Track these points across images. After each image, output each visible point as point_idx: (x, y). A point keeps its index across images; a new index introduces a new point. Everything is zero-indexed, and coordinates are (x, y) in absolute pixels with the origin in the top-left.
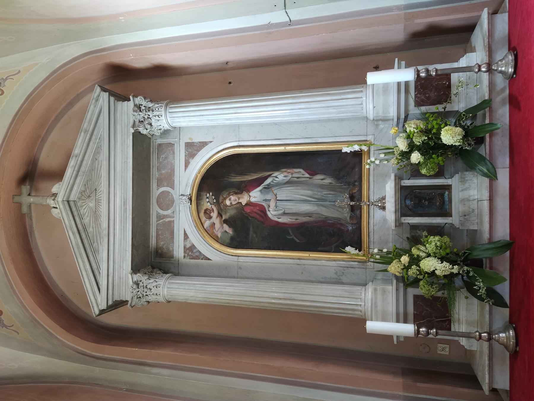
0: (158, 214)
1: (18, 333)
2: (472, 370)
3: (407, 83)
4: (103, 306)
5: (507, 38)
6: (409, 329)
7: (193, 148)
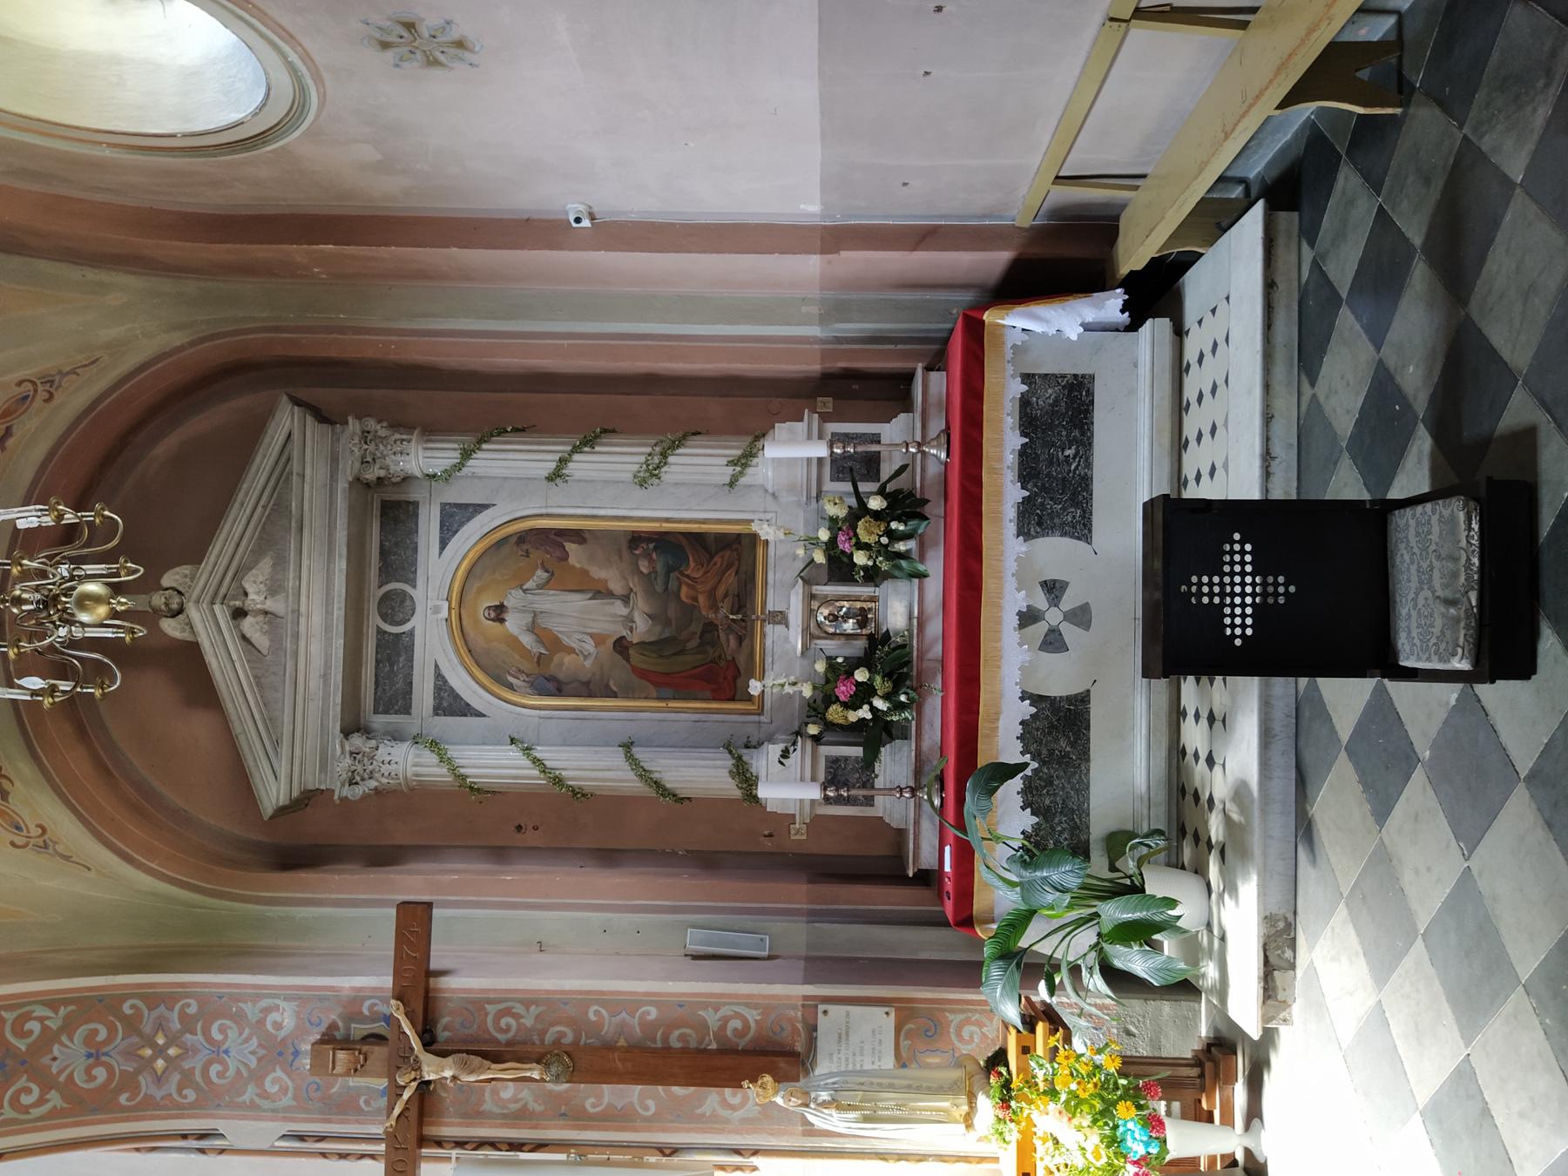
0: (380, 631)
3: (820, 460)
4: (283, 800)
7: (454, 518)
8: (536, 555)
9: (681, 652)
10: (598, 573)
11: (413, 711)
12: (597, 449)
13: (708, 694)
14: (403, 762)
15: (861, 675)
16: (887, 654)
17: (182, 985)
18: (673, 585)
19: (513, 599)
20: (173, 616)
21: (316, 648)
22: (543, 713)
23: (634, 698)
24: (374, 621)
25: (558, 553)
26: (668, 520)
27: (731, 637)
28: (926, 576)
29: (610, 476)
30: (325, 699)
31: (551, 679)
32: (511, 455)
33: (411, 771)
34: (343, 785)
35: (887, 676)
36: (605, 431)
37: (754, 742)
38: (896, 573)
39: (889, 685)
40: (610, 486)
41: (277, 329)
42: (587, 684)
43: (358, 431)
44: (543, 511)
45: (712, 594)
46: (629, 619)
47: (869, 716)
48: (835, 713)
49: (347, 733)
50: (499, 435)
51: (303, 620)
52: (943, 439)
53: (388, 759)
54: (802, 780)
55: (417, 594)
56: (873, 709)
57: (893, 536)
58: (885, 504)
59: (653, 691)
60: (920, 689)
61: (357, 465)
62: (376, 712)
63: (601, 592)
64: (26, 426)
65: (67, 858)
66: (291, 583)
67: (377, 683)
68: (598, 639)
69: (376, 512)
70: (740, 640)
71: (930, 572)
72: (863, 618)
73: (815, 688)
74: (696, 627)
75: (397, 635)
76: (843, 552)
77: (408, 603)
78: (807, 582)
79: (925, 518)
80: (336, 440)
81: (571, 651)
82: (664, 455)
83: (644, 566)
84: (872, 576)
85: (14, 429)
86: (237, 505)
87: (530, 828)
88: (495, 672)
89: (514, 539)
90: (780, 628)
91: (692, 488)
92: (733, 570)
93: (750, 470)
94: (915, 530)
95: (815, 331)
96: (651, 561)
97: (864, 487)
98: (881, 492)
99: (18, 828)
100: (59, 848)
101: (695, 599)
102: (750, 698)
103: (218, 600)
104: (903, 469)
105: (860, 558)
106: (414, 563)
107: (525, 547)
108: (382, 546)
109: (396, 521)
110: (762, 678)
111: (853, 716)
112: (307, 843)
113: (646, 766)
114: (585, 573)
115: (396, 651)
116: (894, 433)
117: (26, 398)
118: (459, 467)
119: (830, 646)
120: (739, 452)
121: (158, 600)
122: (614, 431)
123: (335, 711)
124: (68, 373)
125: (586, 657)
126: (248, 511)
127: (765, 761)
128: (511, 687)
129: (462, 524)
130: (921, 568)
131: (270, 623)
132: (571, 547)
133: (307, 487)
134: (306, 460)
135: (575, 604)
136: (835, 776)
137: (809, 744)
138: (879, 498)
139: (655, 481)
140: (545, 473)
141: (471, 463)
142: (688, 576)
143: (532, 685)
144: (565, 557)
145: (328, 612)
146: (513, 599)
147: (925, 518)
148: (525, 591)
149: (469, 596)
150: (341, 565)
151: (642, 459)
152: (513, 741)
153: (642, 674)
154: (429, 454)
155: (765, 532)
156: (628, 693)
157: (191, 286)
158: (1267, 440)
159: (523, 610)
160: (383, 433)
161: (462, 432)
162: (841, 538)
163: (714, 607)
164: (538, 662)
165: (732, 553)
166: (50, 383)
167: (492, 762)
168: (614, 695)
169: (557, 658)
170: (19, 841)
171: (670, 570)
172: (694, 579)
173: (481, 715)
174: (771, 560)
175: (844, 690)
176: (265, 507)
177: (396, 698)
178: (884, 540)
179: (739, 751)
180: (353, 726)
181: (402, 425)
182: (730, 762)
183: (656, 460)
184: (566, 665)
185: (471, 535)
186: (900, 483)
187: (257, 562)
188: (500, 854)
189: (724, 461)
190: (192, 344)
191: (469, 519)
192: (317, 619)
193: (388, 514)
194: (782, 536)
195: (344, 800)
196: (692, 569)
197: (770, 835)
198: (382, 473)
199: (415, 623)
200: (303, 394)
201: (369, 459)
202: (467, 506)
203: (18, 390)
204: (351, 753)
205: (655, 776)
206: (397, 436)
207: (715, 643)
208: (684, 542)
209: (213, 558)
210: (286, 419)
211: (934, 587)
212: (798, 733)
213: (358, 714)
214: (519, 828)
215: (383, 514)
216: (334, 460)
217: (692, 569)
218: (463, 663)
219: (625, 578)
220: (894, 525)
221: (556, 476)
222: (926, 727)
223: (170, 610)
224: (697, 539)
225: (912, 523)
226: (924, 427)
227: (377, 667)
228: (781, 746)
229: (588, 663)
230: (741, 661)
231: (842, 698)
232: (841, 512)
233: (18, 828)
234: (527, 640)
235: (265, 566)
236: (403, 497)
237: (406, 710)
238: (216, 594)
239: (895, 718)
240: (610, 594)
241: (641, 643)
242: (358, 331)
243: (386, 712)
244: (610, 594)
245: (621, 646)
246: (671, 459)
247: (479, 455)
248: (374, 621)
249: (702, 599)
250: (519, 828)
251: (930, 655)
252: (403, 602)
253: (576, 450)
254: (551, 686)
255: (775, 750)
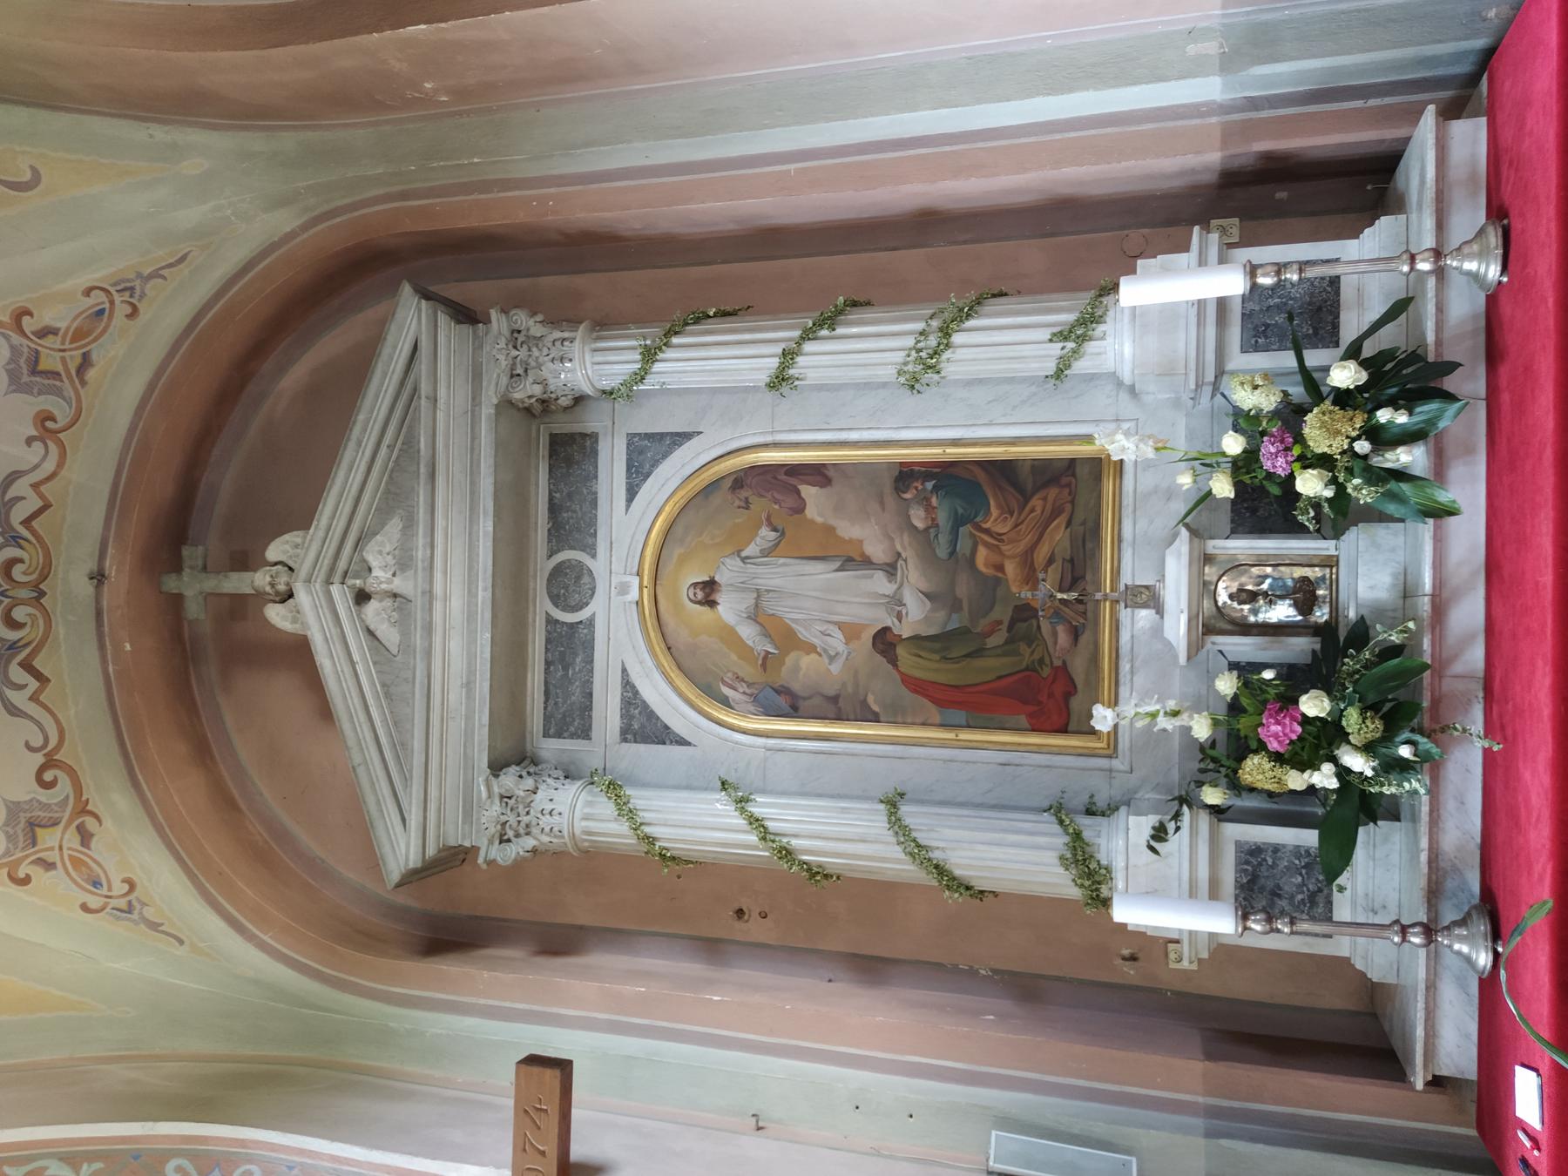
0: (551, 621)
1: (181, 942)
2: (1384, 1036)
3: (1222, 303)
4: (414, 861)
5: (1483, 323)
6: (1221, 922)
7: (646, 453)
8: (760, 505)
9: (978, 653)
10: (849, 530)
11: (594, 734)
12: (840, 331)
13: (1023, 720)
14: (570, 812)
15: (1314, 705)
16: (1368, 666)
17: (243, 1143)
18: (964, 546)
19: (728, 572)
20: (283, 601)
21: (456, 645)
22: (771, 742)
23: (905, 724)
24: (543, 606)
25: (790, 502)
26: (955, 443)
27: (1060, 629)
28: (1451, 512)
29: (860, 375)
30: (469, 717)
31: (782, 691)
32: (714, 352)
33: (580, 825)
34: (491, 842)
35: (1369, 708)
36: (855, 304)
37: (1101, 803)
38: (1392, 508)
39: (1374, 728)
40: (870, 391)
41: (404, 196)
42: (834, 699)
43: (506, 332)
44: (769, 439)
45: (1027, 560)
46: (896, 601)
47: (1333, 784)
48: (1256, 770)
49: (496, 768)
50: (697, 321)
51: (438, 606)
52: (1494, 238)
53: (549, 807)
54: (1193, 894)
55: (598, 566)
56: (1343, 773)
57: (1381, 438)
58: (1363, 377)
59: (934, 712)
60: (1439, 731)
61: (504, 380)
62: (546, 735)
63: (855, 560)
64: (108, 351)
65: (154, 926)
66: (421, 554)
67: (547, 693)
68: (850, 631)
69: (544, 450)
70: (1076, 634)
71: (1462, 503)
72: (1304, 595)
73: (1216, 723)
74: (1002, 613)
75: (573, 626)
76: (1270, 476)
77: (586, 579)
78: (1194, 533)
79: (1450, 397)
80: (479, 347)
81: (811, 648)
82: (946, 332)
83: (918, 518)
84: (1340, 515)
85: (94, 356)
86: (352, 445)
87: (755, 914)
88: (706, 684)
89: (728, 483)
90: (1145, 616)
91: (994, 384)
92: (1061, 520)
93: (1091, 347)
94: (1432, 422)
95: (1209, 89)
96: (929, 508)
97: (1313, 358)
98: (1353, 353)
99: (96, 884)
100: (149, 913)
101: (1000, 568)
102: (1093, 732)
103: (337, 578)
104: (1399, 308)
105: (1310, 484)
106: (593, 522)
107: (744, 493)
108: (551, 499)
109: (569, 462)
110: (1114, 703)
111: (1296, 781)
112: (452, 920)
113: (922, 838)
114: (829, 530)
115: (570, 647)
116: (1365, 264)
117: (101, 312)
118: (640, 376)
119: (1243, 647)
120: (1070, 317)
121: (261, 579)
122: (868, 304)
123: (482, 735)
124: (151, 276)
125: (832, 659)
126: (368, 453)
127: (1122, 842)
128: (726, 702)
129: (655, 464)
130: (1443, 497)
131: (400, 609)
132: (808, 492)
133: (440, 415)
134: (434, 373)
135: (819, 575)
136: (1254, 878)
137: (1204, 819)
138: (1352, 365)
139: (931, 376)
140: (763, 378)
141: (657, 367)
142: (987, 531)
143: (755, 699)
144: (800, 509)
145: (471, 593)
146: (728, 572)
147: (1450, 397)
148: (744, 560)
149: (667, 570)
150: (486, 526)
151: (910, 342)
152: (724, 785)
153: (917, 686)
154: (599, 358)
155: (1121, 446)
156: (895, 715)
157: (288, 141)
158: (376, 795)
159: (741, 588)
160: (537, 330)
161: (641, 321)
162: (1268, 448)
163: (1031, 579)
164: (764, 665)
165: (1065, 491)
166: (128, 293)
167: (697, 822)
168: (875, 718)
169: (790, 660)
170: (94, 902)
171: (958, 522)
172: (998, 537)
173: (683, 742)
174: (1128, 500)
175: (1277, 733)
176: (391, 447)
177: (572, 718)
178: (1362, 447)
179: (1077, 816)
180: (512, 756)
181: (563, 316)
182: (1061, 840)
183: (932, 341)
184: (804, 670)
185: (670, 477)
186: (1388, 338)
187: (383, 525)
188: (712, 948)
189: (1045, 334)
190: (305, 227)
191: (665, 456)
192: (457, 604)
193: (555, 449)
194: (1150, 453)
195: (491, 863)
196: (995, 520)
197: (1133, 958)
198: (537, 390)
199: (596, 607)
200: (453, 291)
201: (519, 371)
202: (661, 436)
203: (90, 301)
204: (502, 797)
205: (936, 855)
206: (557, 334)
207: (1033, 638)
208: (981, 476)
209: (324, 521)
210: (410, 318)
211: (1469, 534)
212: (1183, 800)
213: (524, 737)
214: (740, 913)
215: (553, 453)
216: (477, 376)
217: (995, 520)
218: (659, 666)
219: (892, 539)
220: (1383, 415)
221: (780, 380)
222: (1449, 805)
223: (277, 593)
224: (1003, 472)
225: (1426, 409)
226: (1440, 226)
227: (547, 671)
228: (1153, 820)
229: (835, 668)
230: (1078, 668)
231: (1273, 745)
232: (1262, 400)
233: (96, 884)
234: (748, 632)
235: (394, 527)
236: (576, 428)
237: (585, 733)
238: (332, 569)
239: (1387, 790)
240: (867, 563)
241: (916, 638)
242: (506, 184)
243: (559, 735)
244: (867, 563)
245: (884, 642)
246: (957, 338)
247: (669, 354)
248: (543, 606)
249: (1011, 568)
250: (740, 913)
251: (1458, 668)
252: (578, 578)
253: (808, 335)
254: (782, 701)
255: (1140, 826)
